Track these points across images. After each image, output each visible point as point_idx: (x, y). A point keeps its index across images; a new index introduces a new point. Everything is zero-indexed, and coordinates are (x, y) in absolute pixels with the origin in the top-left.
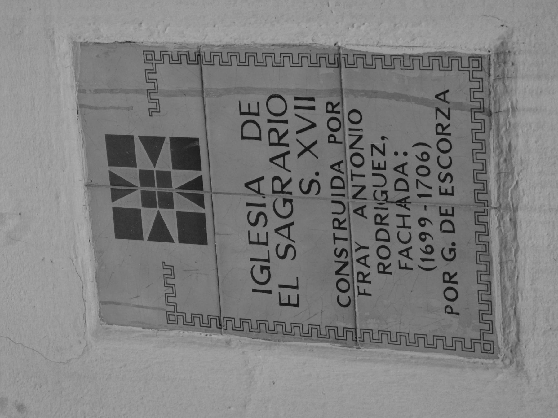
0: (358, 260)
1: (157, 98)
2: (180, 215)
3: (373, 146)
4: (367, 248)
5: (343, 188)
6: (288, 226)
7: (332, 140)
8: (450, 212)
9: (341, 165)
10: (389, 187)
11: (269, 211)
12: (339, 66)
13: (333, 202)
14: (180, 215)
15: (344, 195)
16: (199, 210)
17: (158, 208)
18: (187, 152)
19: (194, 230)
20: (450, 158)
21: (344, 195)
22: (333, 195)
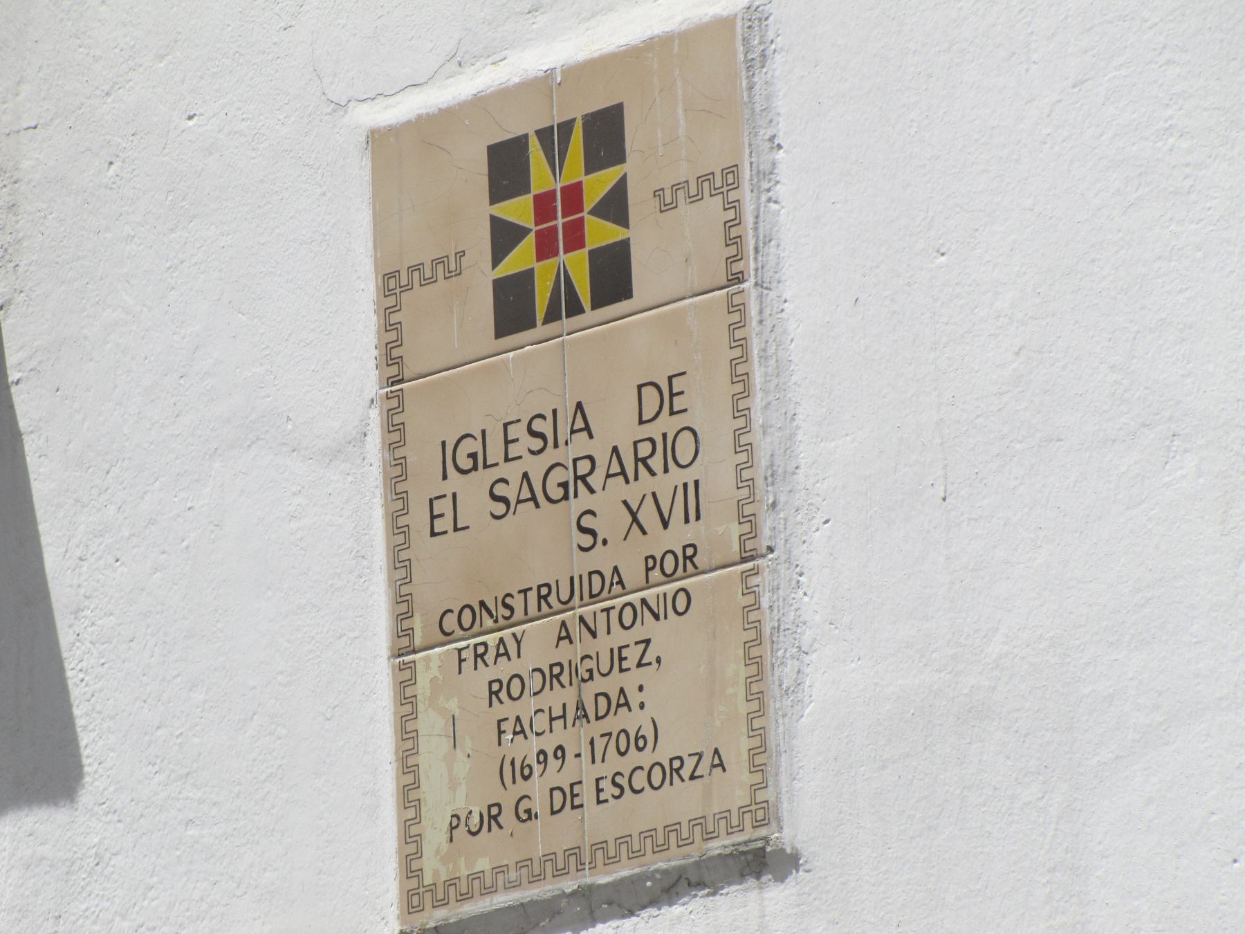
0: (501, 640)
1: (588, 848)
2: (530, 274)
3: (648, 642)
4: (519, 656)
5: (591, 596)
6: (533, 498)
7: (651, 563)
8: (577, 802)
9: (619, 586)
10: (599, 684)
11: (551, 456)
12: (744, 560)
13: (572, 579)
14: (530, 274)
15: (582, 599)
16: (540, 315)
17: (585, 214)
18: (613, 278)
19: (513, 310)
20: (642, 790)
21: (582, 599)
22: (581, 577)
